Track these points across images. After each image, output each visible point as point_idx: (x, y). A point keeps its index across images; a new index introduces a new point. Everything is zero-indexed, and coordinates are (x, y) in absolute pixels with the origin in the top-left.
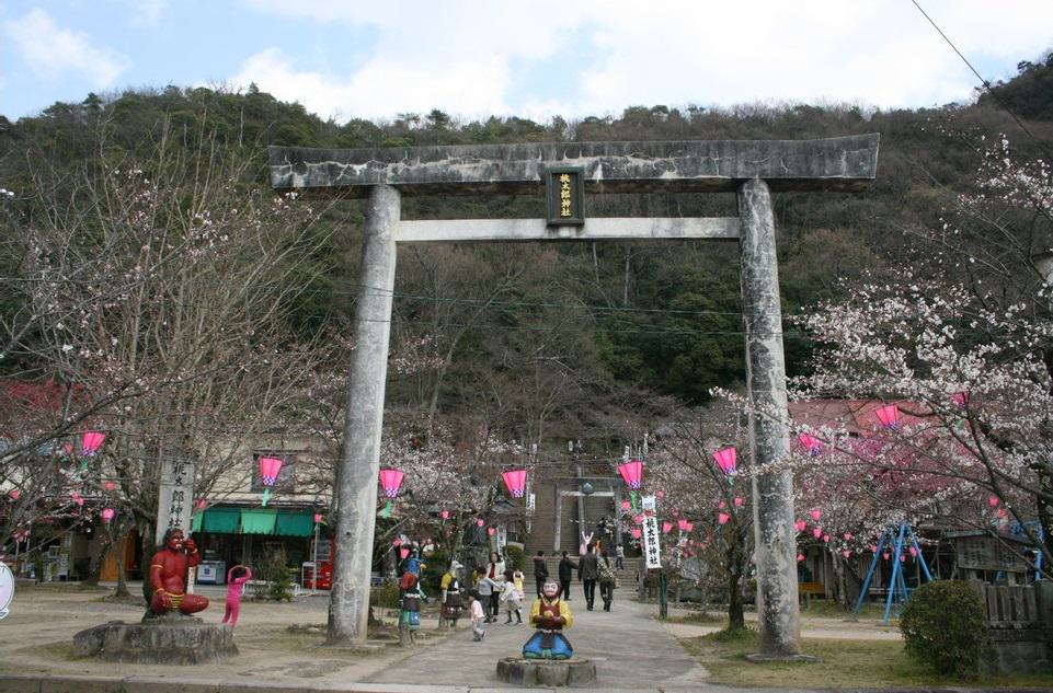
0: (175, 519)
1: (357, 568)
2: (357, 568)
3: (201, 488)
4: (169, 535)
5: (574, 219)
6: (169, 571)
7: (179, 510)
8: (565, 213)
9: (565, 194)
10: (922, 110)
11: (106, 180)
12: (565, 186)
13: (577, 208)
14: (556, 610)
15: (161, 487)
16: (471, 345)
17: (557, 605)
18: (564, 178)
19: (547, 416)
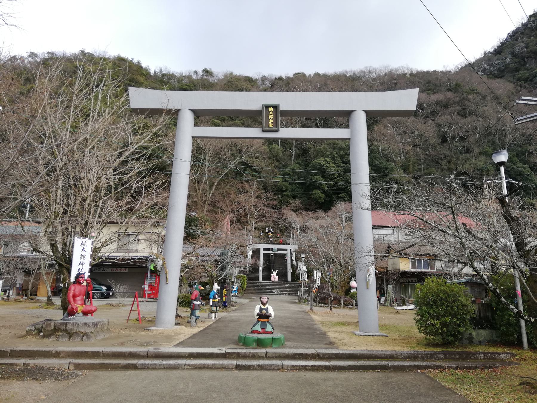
0: (81, 268)
1: (171, 290)
2: (171, 290)
3: (95, 250)
4: (79, 276)
5: (275, 129)
6: (77, 293)
7: (83, 263)
8: (271, 125)
9: (271, 117)
10: (435, 72)
11: (533, 371)
12: (271, 113)
13: (276, 124)
14: (267, 310)
15: (369, 194)
16: (224, 175)
17: (267, 308)
18: (271, 109)
19: (38, 263)
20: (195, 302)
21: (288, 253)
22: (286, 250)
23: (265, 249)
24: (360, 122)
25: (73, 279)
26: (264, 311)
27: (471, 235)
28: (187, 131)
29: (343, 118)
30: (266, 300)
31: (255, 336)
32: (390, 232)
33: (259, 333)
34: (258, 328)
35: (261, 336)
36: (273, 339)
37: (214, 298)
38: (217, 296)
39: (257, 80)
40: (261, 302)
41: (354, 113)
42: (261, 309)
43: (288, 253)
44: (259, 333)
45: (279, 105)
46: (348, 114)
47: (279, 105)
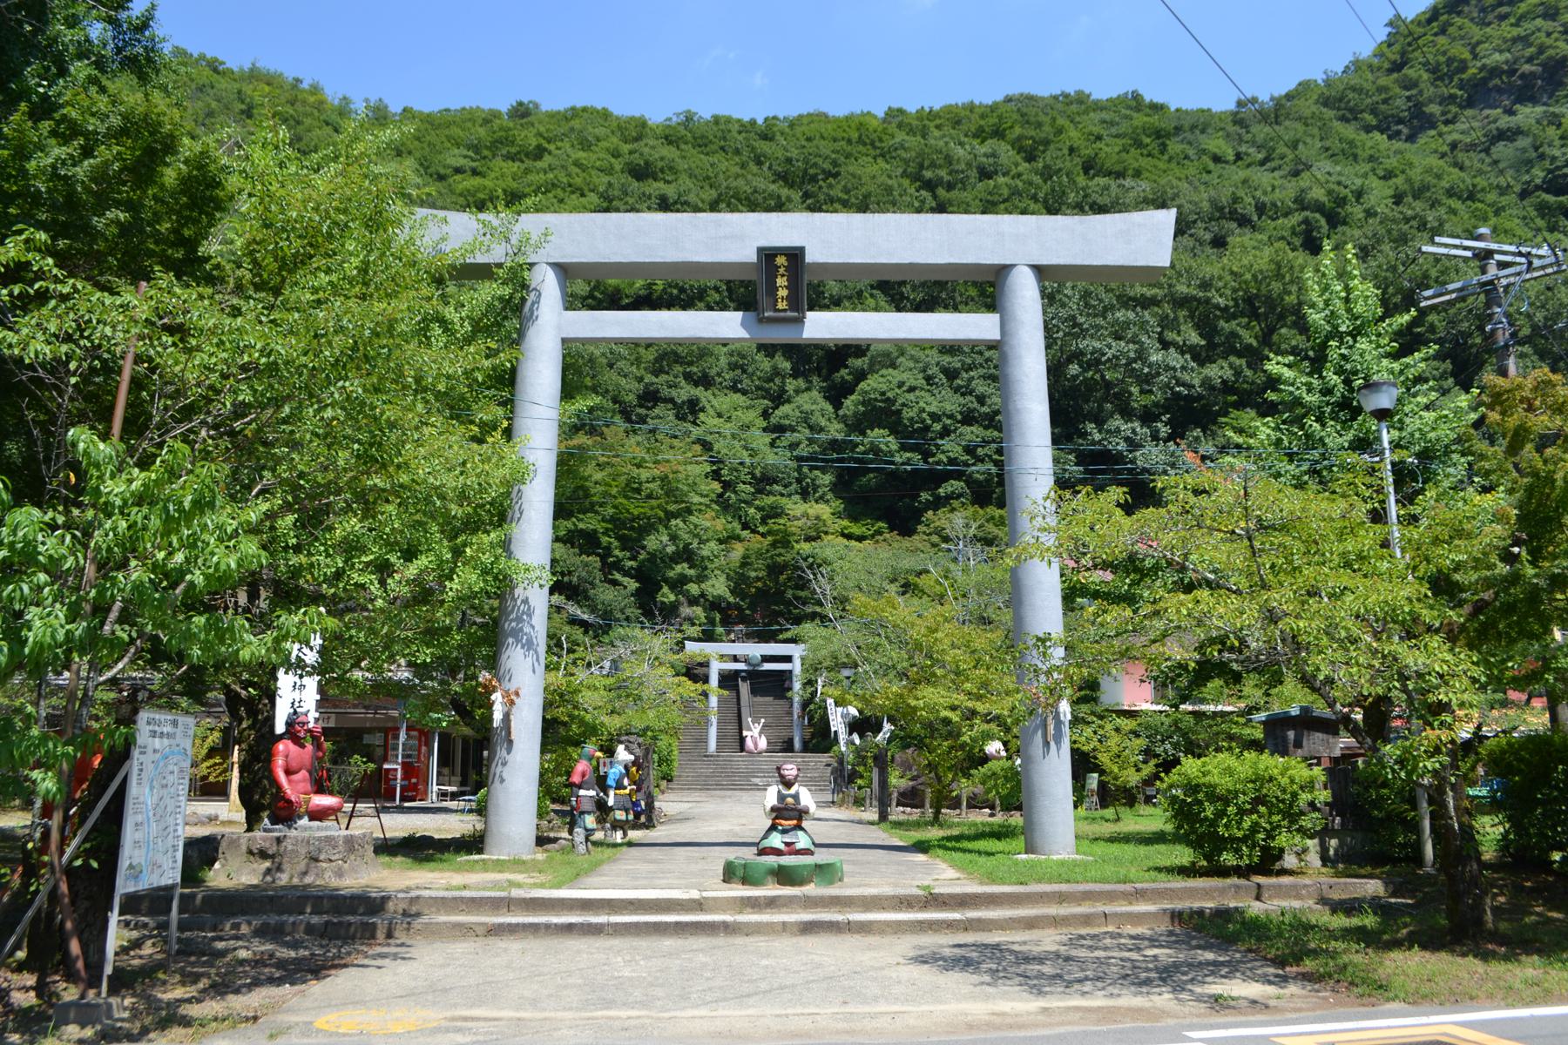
8: (782, 305)
9: (781, 281)
12: (782, 270)
14: (796, 797)
20: (582, 792)
21: (796, 667)
22: (788, 659)
23: (722, 657)
24: (1025, 295)
25: (280, 728)
26: (790, 800)
27: (1331, 562)
28: (553, 325)
29: (983, 288)
30: (794, 772)
31: (771, 860)
32: (516, 893)
33: (778, 852)
34: (776, 841)
35: (787, 860)
36: (818, 867)
37: (620, 786)
38: (626, 782)
39: (344, 111)
40: (782, 776)
41: (1015, 270)
42: (781, 798)
43: (796, 667)
44: (778, 852)
45: (802, 250)
46: (1001, 272)
47: (802, 250)
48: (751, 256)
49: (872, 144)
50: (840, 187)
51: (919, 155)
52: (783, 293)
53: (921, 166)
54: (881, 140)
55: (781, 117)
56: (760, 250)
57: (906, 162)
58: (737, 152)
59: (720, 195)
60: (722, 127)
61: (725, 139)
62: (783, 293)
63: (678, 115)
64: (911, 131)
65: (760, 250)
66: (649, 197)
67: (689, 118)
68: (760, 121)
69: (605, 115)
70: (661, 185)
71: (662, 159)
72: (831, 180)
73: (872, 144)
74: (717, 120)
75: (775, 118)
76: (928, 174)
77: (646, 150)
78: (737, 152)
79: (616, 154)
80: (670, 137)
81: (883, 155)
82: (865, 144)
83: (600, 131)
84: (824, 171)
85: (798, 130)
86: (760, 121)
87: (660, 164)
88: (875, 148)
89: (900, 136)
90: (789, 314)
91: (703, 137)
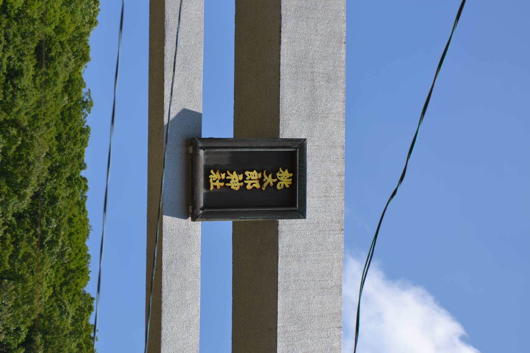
12: (269, 180)
45: (301, 213)
47: (301, 213)
48: (290, 129)
49: (66, 283)
50: (30, 250)
51: (57, 328)
52: (235, 181)
53: (45, 333)
54: (69, 290)
55: (87, 194)
56: (301, 144)
57: (50, 318)
58: (61, 150)
59: (25, 130)
60: (79, 137)
61: (68, 138)
62: (235, 181)
63: (89, 93)
64: (75, 320)
65: (301, 144)
66: (20, 60)
67: (86, 104)
68: (83, 173)
69: (92, 23)
70: (32, 72)
71: (56, 74)
72: (36, 240)
73: (66, 283)
74: (85, 131)
75: (86, 187)
76: (38, 338)
77: (64, 59)
78: (61, 150)
79: (58, 30)
80: (73, 84)
81: (54, 294)
82: (65, 276)
83: (79, 16)
84: (44, 233)
85: (76, 210)
86: (83, 173)
87: (51, 72)
88: (61, 286)
89: (71, 310)
90: (202, 192)
91: (71, 117)
